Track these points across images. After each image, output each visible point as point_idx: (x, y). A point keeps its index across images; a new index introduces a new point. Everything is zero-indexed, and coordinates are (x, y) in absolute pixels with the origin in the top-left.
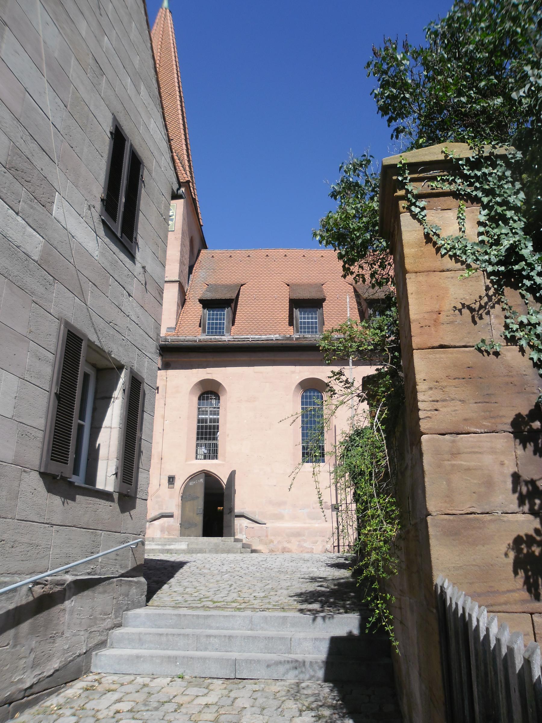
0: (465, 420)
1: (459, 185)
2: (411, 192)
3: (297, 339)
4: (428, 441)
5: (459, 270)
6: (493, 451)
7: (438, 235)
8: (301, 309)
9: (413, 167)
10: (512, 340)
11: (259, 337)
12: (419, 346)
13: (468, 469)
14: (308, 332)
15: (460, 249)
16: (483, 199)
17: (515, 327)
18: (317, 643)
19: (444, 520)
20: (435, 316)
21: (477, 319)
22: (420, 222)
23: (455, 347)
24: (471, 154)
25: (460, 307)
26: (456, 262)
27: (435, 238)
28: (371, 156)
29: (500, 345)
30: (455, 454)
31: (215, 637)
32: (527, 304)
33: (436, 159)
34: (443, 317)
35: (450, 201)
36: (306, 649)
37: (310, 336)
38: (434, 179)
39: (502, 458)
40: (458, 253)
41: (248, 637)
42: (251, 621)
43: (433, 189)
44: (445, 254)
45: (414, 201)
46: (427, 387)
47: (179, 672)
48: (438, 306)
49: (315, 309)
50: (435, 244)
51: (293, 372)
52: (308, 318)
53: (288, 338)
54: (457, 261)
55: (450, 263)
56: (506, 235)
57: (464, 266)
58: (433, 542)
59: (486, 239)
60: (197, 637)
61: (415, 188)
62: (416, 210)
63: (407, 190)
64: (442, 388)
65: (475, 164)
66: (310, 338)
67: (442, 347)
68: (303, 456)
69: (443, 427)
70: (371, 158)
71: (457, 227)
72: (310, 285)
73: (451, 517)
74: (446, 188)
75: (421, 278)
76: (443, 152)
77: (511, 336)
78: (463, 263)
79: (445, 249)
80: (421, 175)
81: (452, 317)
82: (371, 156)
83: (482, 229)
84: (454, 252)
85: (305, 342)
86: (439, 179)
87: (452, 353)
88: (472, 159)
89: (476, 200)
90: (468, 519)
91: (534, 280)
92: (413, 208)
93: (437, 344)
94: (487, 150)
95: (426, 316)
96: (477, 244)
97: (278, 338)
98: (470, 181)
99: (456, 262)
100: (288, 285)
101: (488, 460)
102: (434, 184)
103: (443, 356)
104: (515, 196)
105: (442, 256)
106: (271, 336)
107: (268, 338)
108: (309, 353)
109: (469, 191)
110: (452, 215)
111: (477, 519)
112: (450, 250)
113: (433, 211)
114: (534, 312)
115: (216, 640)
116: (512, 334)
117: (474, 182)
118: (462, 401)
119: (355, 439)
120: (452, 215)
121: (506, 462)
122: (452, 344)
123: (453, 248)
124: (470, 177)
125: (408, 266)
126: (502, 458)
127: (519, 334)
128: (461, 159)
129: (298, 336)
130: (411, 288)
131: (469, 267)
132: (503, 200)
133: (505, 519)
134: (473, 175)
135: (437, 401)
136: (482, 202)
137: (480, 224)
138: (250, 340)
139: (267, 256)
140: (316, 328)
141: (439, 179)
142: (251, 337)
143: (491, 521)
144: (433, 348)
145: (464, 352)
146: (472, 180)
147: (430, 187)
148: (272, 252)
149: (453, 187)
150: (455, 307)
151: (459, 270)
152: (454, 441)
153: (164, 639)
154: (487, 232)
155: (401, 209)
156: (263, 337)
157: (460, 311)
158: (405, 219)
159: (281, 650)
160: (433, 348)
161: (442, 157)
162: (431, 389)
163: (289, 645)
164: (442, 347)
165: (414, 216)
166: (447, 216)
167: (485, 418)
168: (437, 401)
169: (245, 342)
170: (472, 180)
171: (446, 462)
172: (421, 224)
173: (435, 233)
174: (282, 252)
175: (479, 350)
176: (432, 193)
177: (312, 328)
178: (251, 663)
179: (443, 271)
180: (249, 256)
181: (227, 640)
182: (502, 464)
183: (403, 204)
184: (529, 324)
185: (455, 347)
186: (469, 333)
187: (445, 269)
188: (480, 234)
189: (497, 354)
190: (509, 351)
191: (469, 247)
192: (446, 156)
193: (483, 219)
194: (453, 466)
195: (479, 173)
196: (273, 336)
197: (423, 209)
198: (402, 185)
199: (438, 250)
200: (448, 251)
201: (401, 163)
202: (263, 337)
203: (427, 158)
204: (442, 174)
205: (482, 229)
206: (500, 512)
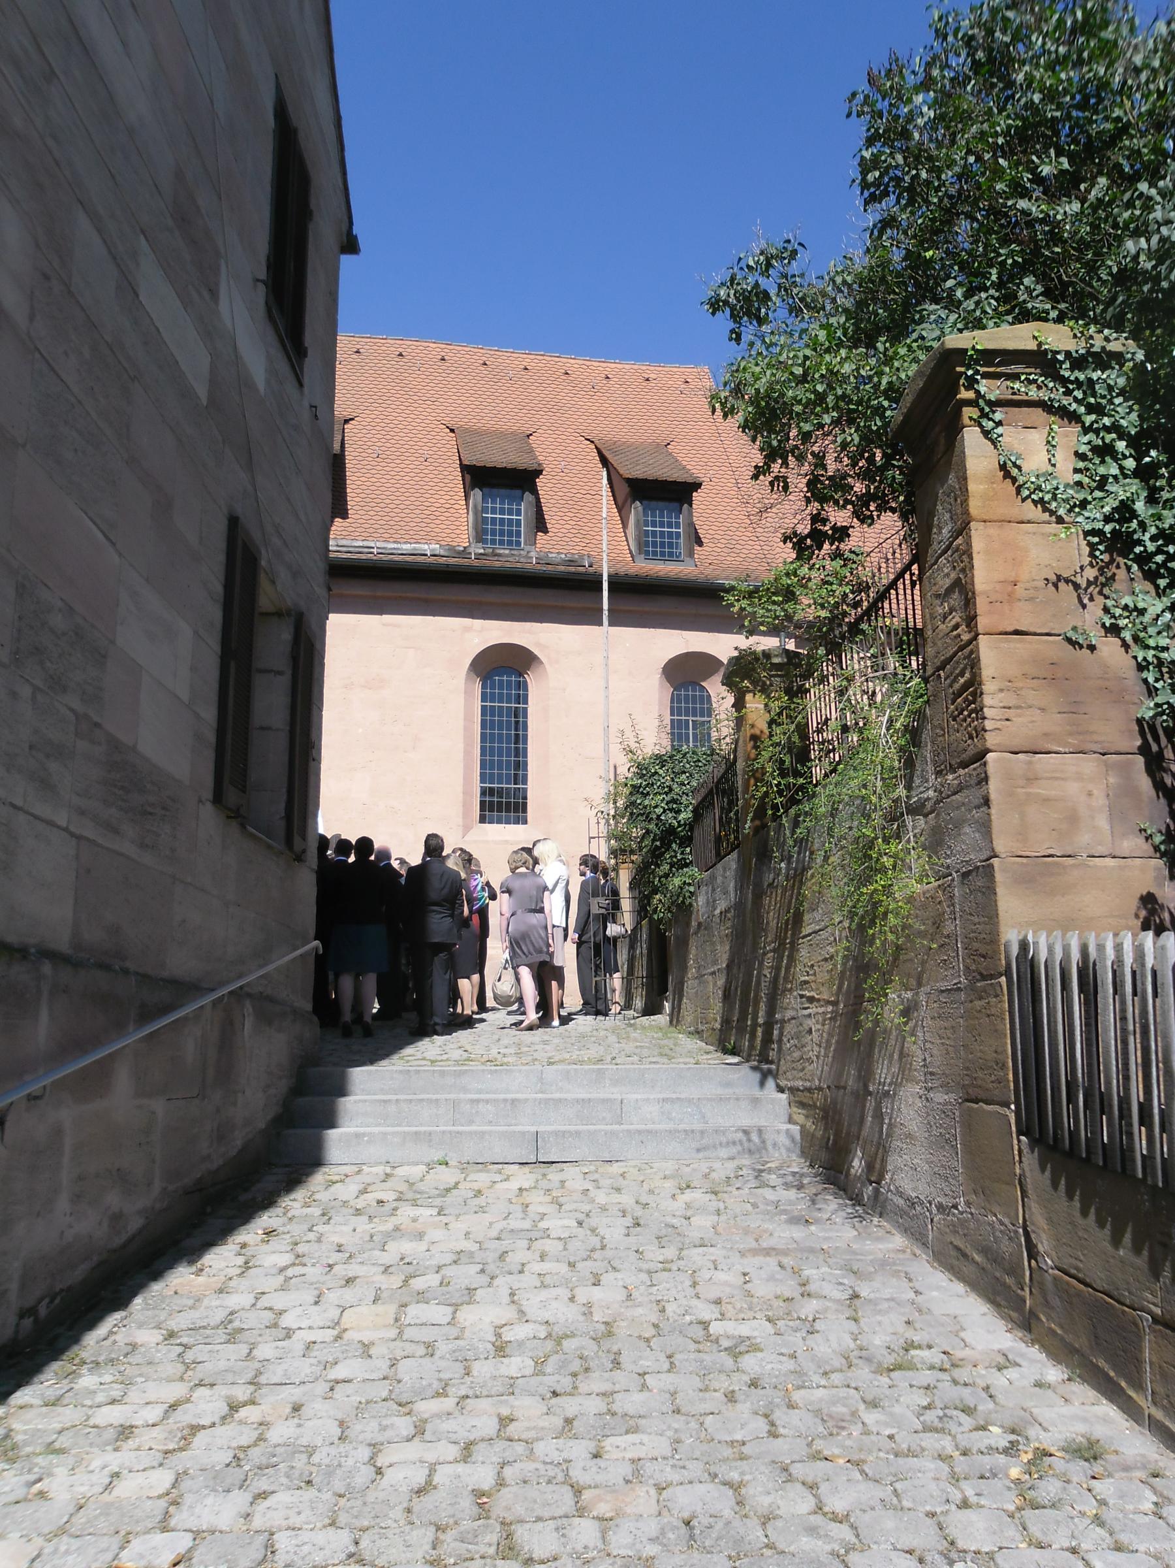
0: (1045, 734)
1: (1056, 394)
2: (983, 397)
3: (479, 556)
4: (998, 760)
5: (1044, 522)
6: (1079, 777)
7: (1019, 468)
8: (486, 490)
9: (988, 356)
10: (1114, 630)
11: (395, 546)
12: (987, 630)
13: (1046, 800)
14: (502, 542)
15: (1048, 492)
16: (1083, 418)
17: (1118, 612)
18: (668, 1106)
19: (1014, 863)
20: (1010, 588)
21: (1086, 601)
22: (994, 443)
23: (1035, 634)
24: (1078, 347)
25: (1054, 578)
26: (1044, 511)
27: (1015, 472)
28: (800, 244)
29: (1096, 636)
30: (1032, 779)
31: (487, 1101)
32: (1132, 579)
33: (1022, 347)
34: (1020, 590)
35: (1038, 414)
36: (648, 1116)
37: (507, 552)
38: (1015, 377)
39: (1090, 787)
40: (1047, 497)
41: (540, 1101)
42: (541, 1079)
43: (1014, 394)
44: (1029, 497)
45: (987, 409)
46: (996, 688)
47: (437, 1155)
48: (1013, 574)
49: (518, 492)
50: (1014, 480)
51: (468, 629)
52: (502, 512)
53: (459, 552)
54: (1045, 510)
55: (1036, 513)
56: (1115, 477)
57: (1054, 519)
58: (1000, 890)
59: (1086, 480)
60: (455, 1104)
61: (990, 389)
62: (989, 425)
63: (978, 392)
64: (1017, 691)
65: (1078, 363)
66: (507, 556)
67: (1017, 632)
68: (482, 808)
69: (1016, 744)
70: (800, 248)
71: (1044, 456)
72: (502, 435)
73: (1024, 860)
74: (1034, 393)
75: (993, 530)
76: (1035, 338)
77: (1111, 624)
78: (1052, 513)
79: (1028, 489)
80: (999, 370)
81: (1032, 591)
82: (800, 244)
83: (1081, 465)
84: (1041, 495)
85: (497, 564)
86: (1023, 378)
87: (1030, 643)
88: (1074, 354)
89: (1074, 417)
90: (1045, 863)
91: (1145, 546)
92: (984, 422)
93: (1010, 629)
94: (1098, 343)
95: (998, 587)
96: (1072, 487)
97: (437, 552)
98: (1067, 388)
99: (1044, 511)
100: (452, 431)
101: (1073, 788)
102: (1017, 385)
103: (1018, 645)
104: (1044, 347)
105: (1024, 500)
106: (422, 546)
107: (415, 549)
108: (505, 588)
109: (1065, 403)
110: (1037, 438)
111: (1057, 863)
112: (1034, 493)
113: (1011, 429)
114: (1141, 592)
115: (489, 1107)
116: (1113, 621)
117: (1073, 390)
118: (1043, 710)
119: (656, 773)
120: (1037, 438)
121: (1095, 792)
122: (1032, 629)
123: (1039, 488)
124: (1067, 380)
125: (973, 511)
126: (1090, 787)
127: (1122, 622)
128: (1058, 352)
129: (482, 551)
130: (977, 544)
131: (1060, 520)
132: (1113, 423)
133: (1091, 863)
134: (1072, 378)
135: (1009, 708)
136: (1083, 423)
137: (1081, 457)
138: (375, 551)
139: (401, 355)
140: (518, 534)
141: (1023, 378)
142: (379, 544)
143: (1073, 865)
144: (1006, 633)
145: (1047, 642)
146: (1071, 387)
147: (1010, 391)
148: (409, 346)
149: (1044, 395)
150: (1047, 579)
151: (1044, 522)
152: (1030, 763)
153: (392, 1108)
154: (1087, 469)
155: (966, 421)
156: (405, 546)
157: (1056, 586)
158: (971, 437)
159: (604, 1119)
160: (1006, 633)
161: (1032, 346)
162: (1001, 690)
163: (619, 1111)
164: (1017, 632)
165: (986, 434)
166: (1030, 437)
167: (1071, 734)
168: (1009, 708)
169: (363, 557)
170: (1071, 387)
171: (1019, 790)
172: (995, 447)
173: (1015, 465)
174: (435, 348)
175: (1069, 640)
176: (1012, 400)
177: (510, 534)
178: (564, 1136)
179: (1023, 522)
180: (358, 352)
181: (509, 1107)
182: (1090, 794)
183: (968, 412)
184: (1136, 609)
185: (1035, 634)
186: (1054, 616)
187: (1025, 519)
188: (1076, 471)
189: (1092, 648)
190: (1105, 644)
191: (1062, 488)
192: (1040, 345)
193: (1084, 449)
194: (1028, 794)
195: (1082, 377)
196: (426, 547)
197: (999, 424)
198: (971, 383)
199: (1018, 492)
200: (1031, 493)
201: (973, 348)
202: (405, 546)
203: (1011, 345)
204: (1028, 370)
205: (1081, 465)
206: (1085, 855)
